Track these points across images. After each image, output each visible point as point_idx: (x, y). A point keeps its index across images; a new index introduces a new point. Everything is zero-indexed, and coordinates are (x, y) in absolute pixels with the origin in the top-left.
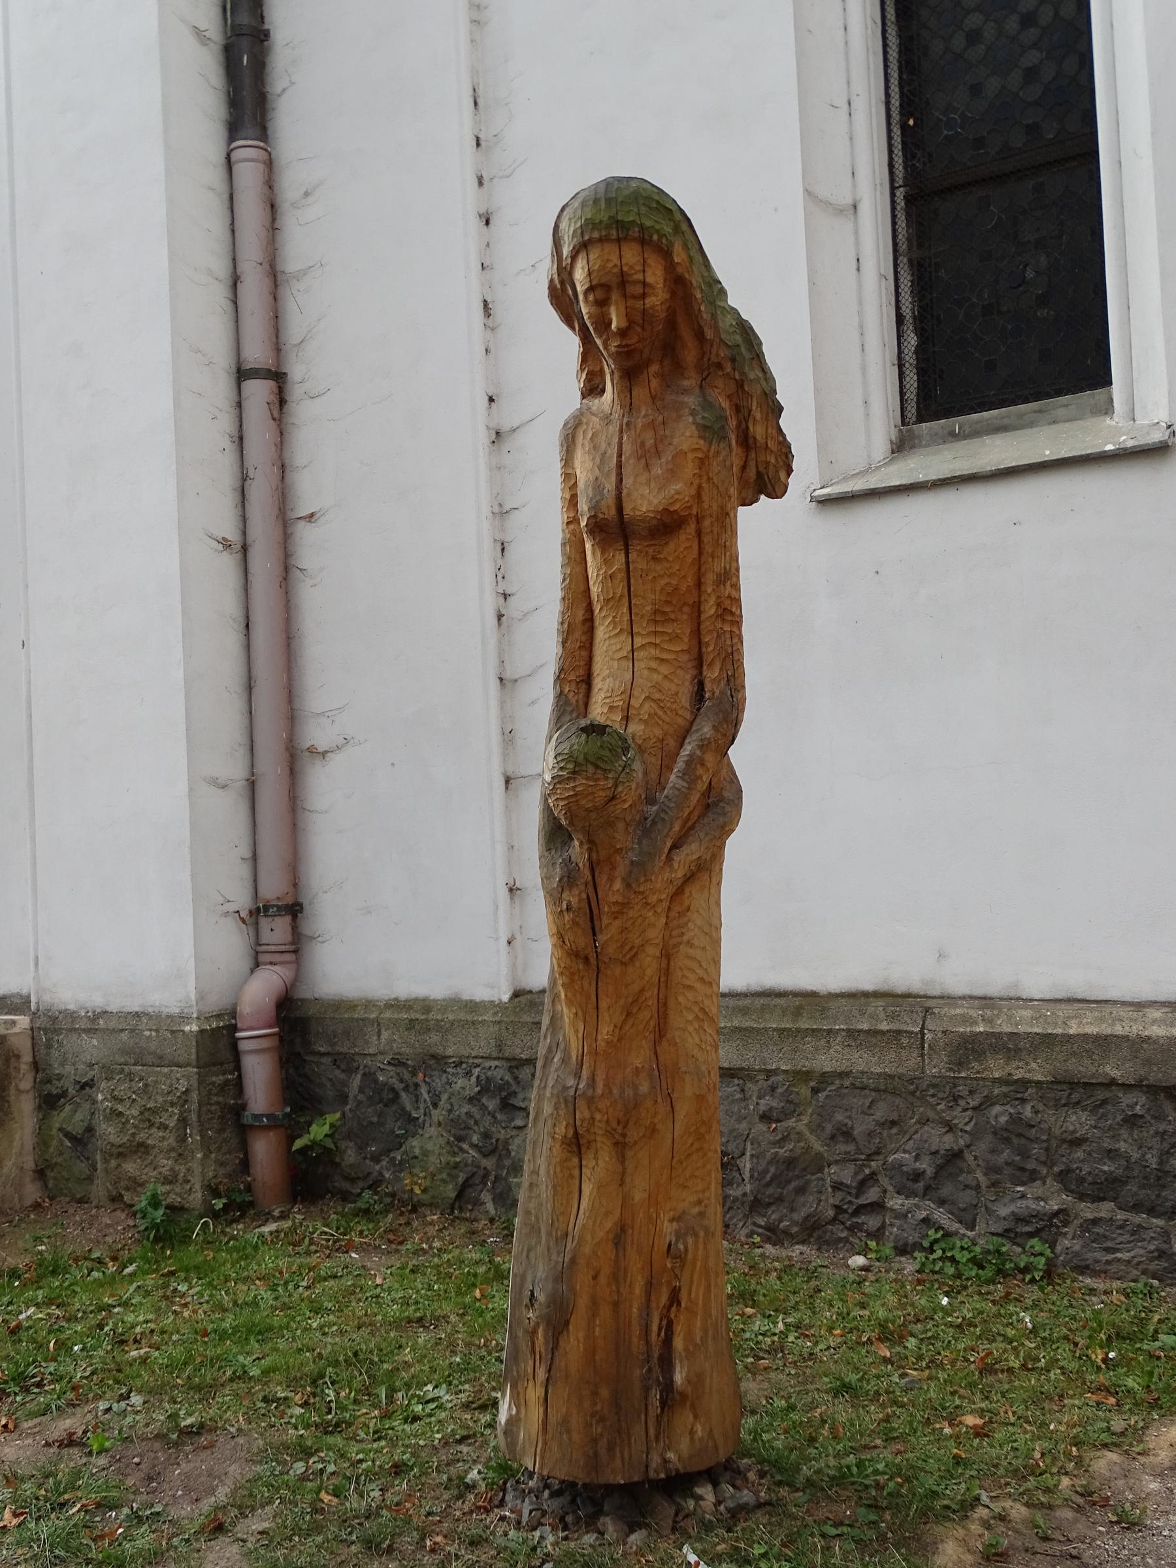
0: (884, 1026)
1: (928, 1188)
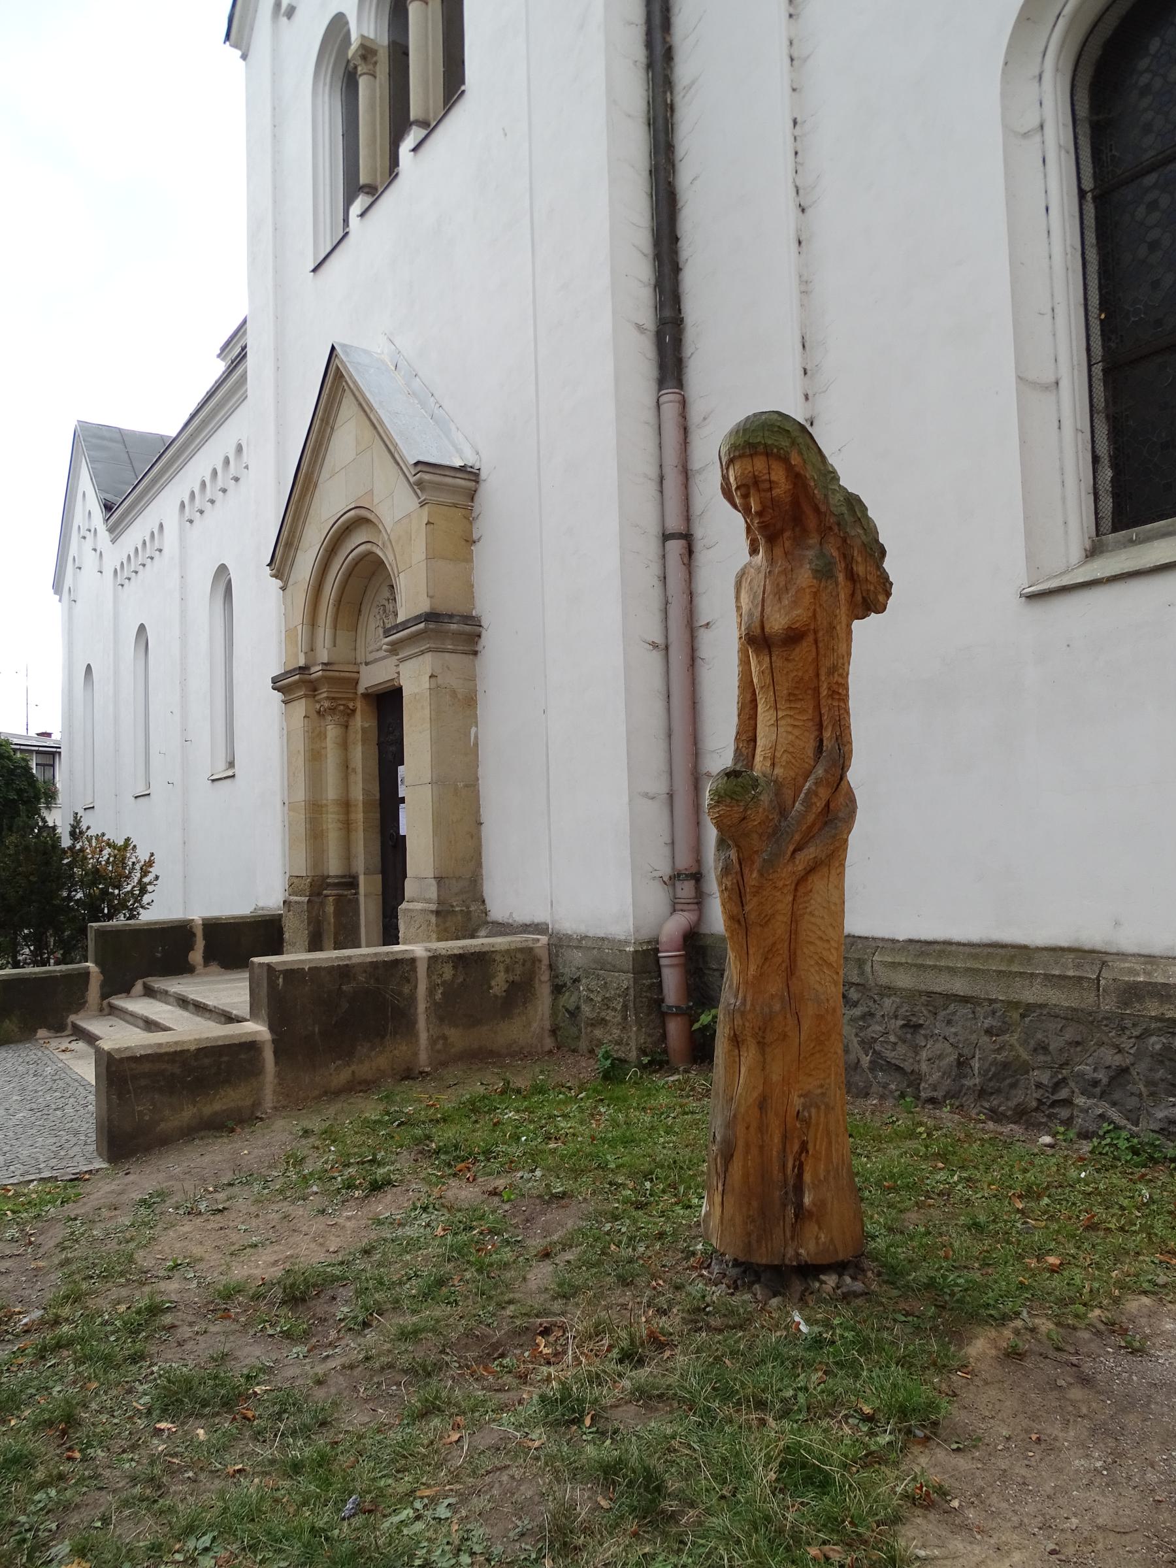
0: (1071, 973)
1: (1103, 1093)
